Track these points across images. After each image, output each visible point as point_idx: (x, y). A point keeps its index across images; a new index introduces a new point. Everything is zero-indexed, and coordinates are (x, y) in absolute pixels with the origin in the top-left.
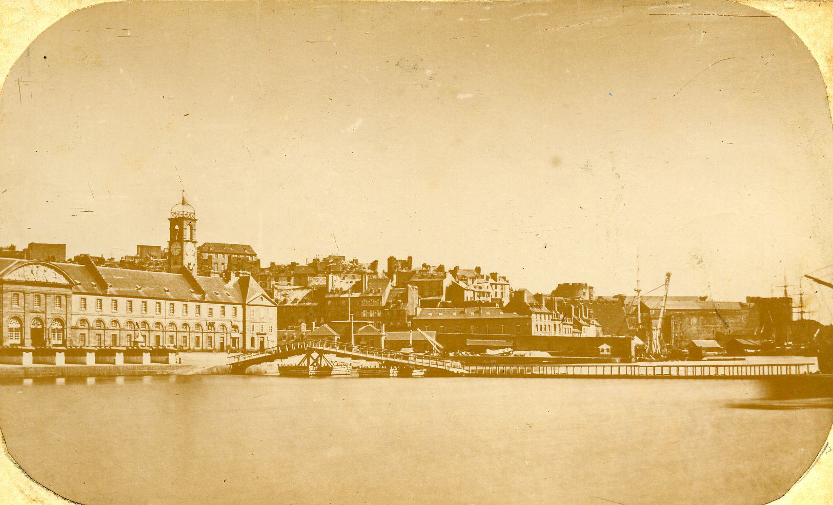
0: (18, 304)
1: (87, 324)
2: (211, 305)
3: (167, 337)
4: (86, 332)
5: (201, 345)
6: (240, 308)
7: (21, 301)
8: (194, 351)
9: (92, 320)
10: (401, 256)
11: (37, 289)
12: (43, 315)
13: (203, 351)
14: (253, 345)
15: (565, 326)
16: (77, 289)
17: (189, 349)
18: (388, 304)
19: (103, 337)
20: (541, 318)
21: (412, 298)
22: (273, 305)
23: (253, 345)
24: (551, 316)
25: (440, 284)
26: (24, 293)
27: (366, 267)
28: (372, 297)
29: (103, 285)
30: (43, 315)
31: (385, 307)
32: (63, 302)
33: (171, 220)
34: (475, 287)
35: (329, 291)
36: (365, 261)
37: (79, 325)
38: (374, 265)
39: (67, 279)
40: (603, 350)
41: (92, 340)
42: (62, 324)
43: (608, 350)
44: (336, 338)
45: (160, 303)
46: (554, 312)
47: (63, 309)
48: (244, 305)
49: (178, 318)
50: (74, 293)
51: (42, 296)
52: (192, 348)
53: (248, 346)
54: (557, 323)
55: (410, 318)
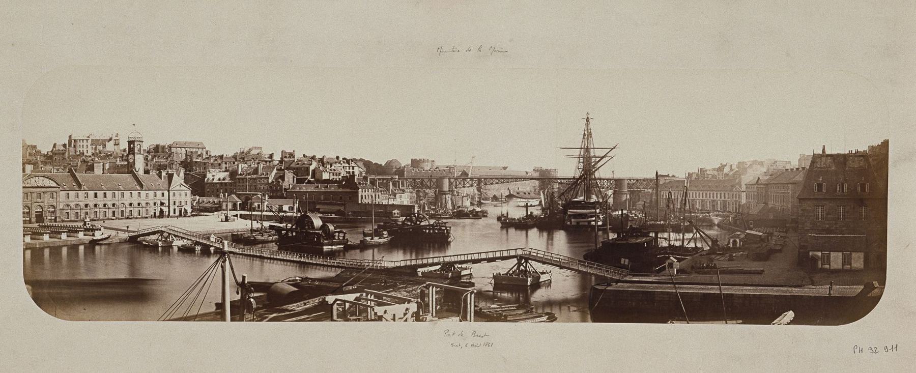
0: (27, 199)
1: (69, 207)
2: (147, 192)
3: (120, 211)
4: (69, 211)
5: (141, 214)
6: (166, 193)
7: (29, 198)
8: (137, 218)
9: (72, 205)
10: (289, 151)
11: (38, 190)
12: (42, 204)
13: (142, 217)
14: (174, 213)
15: (382, 195)
16: (64, 188)
17: (134, 217)
18: (273, 182)
19: (79, 214)
20: (365, 191)
21: (289, 178)
22: (187, 189)
23: (174, 213)
24: (373, 190)
25: (308, 169)
26: (31, 193)
27: (266, 157)
28: (263, 178)
29: (80, 185)
30: (42, 204)
31: (271, 184)
32: (55, 196)
33: (128, 142)
34: (331, 170)
35: (239, 173)
36: (266, 153)
37: (65, 208)
38: (271, 156)
39: (57, 183)
40: (395, 214)
41: (72, 215)
42: (55, 208)
43: (398, 214)
44: (238, 203)
45: (115, 193)
46: (375, 187)
47: (55, 200)
48: (169, 191)
49: (126, 200)
50: (61, 191)
51: (42, 194)
52: (135, 217)
53: (172, 214)
54: (377, 194)
55: (286, 190)
